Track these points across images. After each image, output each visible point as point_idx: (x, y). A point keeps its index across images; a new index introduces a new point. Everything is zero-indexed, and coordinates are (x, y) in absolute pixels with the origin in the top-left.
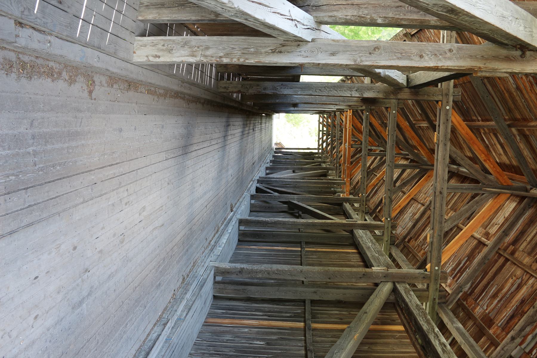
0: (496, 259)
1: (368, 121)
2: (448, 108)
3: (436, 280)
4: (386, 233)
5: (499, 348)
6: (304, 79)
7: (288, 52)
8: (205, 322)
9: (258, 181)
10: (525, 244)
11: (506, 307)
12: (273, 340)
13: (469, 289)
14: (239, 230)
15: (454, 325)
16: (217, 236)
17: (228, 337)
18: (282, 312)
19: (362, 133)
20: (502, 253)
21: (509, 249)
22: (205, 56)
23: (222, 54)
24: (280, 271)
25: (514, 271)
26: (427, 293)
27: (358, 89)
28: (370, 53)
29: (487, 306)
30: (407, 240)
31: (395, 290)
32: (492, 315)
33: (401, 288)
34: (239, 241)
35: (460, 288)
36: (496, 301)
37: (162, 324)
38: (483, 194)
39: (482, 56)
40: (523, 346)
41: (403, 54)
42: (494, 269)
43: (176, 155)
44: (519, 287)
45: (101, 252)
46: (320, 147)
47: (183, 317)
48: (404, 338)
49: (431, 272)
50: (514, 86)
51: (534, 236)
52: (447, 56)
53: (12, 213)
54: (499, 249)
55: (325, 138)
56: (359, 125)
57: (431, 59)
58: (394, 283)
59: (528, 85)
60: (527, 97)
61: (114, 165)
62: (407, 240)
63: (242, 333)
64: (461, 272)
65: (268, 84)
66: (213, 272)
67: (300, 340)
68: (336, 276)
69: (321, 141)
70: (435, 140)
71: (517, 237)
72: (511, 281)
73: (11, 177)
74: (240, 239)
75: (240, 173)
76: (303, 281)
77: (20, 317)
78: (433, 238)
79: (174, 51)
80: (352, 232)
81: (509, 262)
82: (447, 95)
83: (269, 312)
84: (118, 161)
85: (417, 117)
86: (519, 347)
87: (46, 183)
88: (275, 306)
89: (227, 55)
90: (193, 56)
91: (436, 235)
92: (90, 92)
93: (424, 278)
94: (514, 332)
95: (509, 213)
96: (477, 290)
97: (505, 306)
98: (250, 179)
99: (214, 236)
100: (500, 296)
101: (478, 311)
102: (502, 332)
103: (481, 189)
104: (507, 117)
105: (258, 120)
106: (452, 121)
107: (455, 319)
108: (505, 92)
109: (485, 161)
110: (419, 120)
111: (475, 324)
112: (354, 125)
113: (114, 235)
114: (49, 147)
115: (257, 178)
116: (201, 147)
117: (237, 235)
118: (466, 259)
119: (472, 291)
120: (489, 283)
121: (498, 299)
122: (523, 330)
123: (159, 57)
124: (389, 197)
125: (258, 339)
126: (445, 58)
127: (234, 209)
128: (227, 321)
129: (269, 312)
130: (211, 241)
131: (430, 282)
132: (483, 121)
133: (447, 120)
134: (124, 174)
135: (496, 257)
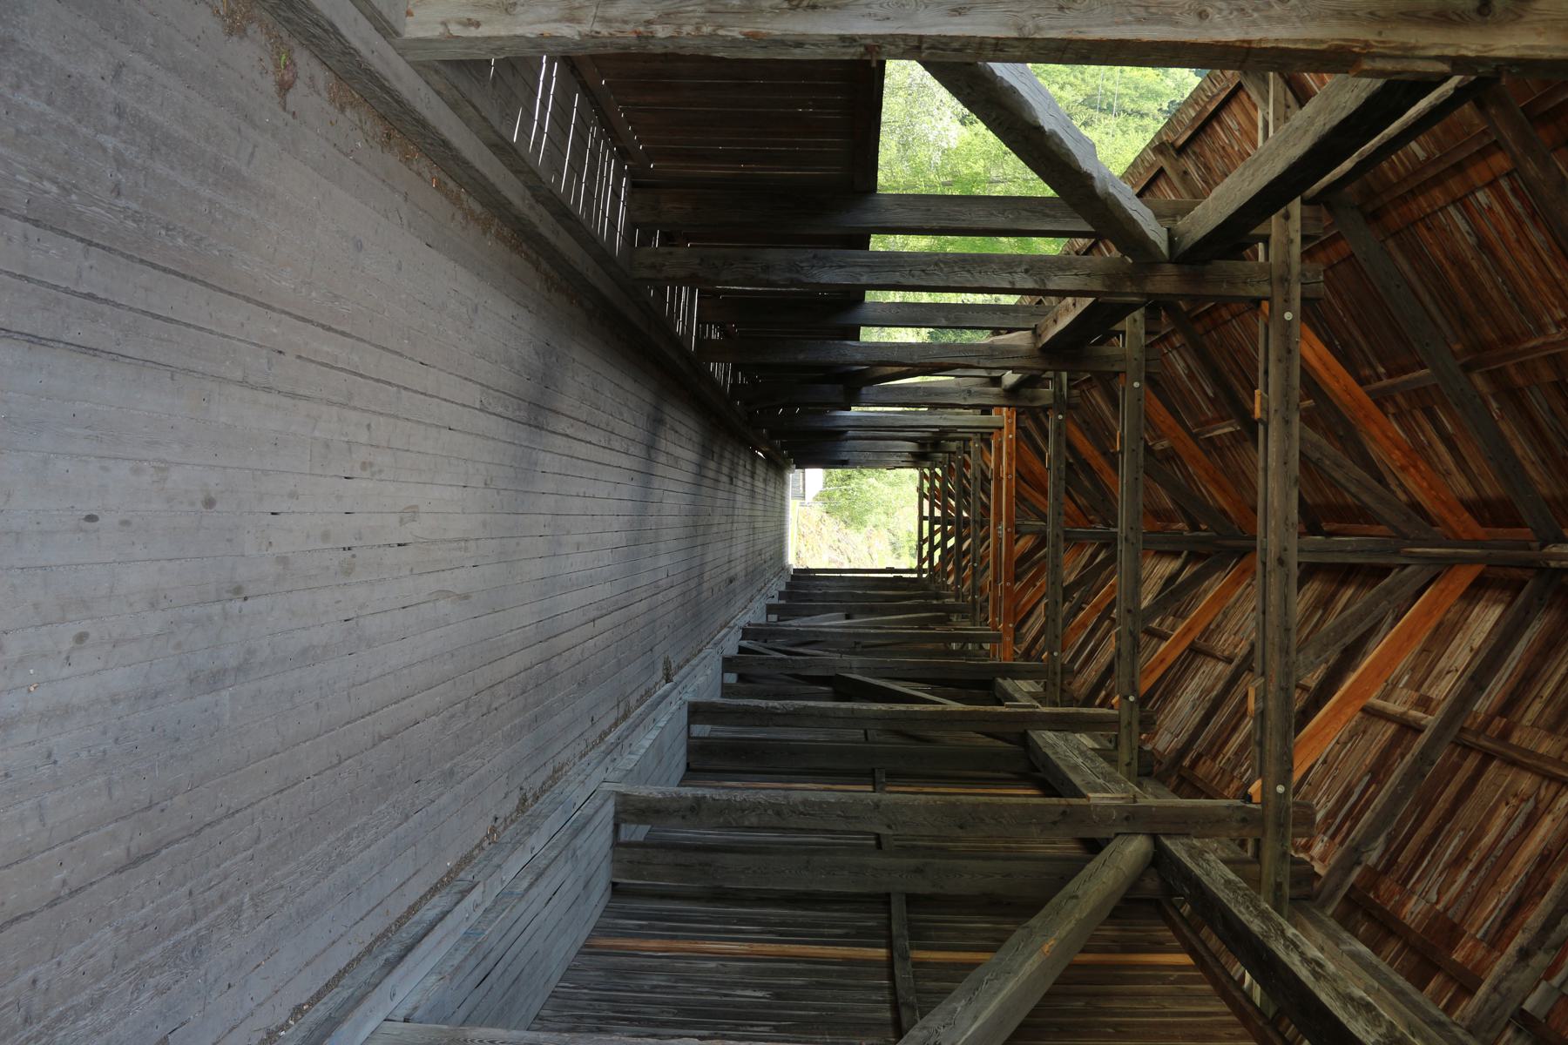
0: (1451, 757)
1: (1063, 439)
2: (1288, 316)
3: (1281, 825)
4: (1124, 741)
5: (1483, 990)
6: (878, 243)
7: (835, 7)
8: (585, 946)
9: (747, 633)
10: (1537, 707)
11: (1495, 883)
12: (794, 987)
13: (1381, 857)
14: (689, 737)
15: (1344, 947)
16: (623, 725)
17: (656, 980)
18: (819, 926)
19: (1044, 493)
20: (1470, 738)
21: (1492, 727)
22: (606, 21)
23: (651, 15)
24: (813, 804)
25: (1512, 782)
26: (1256, 867)
27: (1032, 267)
28: (1061, 8)
29: (1439, 893)
30: (1186, 762)
31: (1159, 859)
32: (1454, 915)
33: (1176, 847)
34: (688, 768)
35: (1353, 856)
36: (1464, 874)
37: (456, 889)
38: (1406, 566)
39: (1371, 13)
40: (1556, 981)
41: (1153, 10)
42: (1452, 789)
43: (509, 414)
44: (1531, 822)
45: (283, 560)
46: (926, 566)
47: (519, 890)
48: (1193, 980)
49: (1264, 802)
50: (1471, 240)
51: (1562, 682)
52: (1272, 13)
53: (40, 283)
54: (1463, 729)
55: (937, 538)
56: (1036, 466)
57: (1229, 22)
58: (1154, 837)
59: (1508, 226)
60: (1509, 264)
61: (336, 331)
62: (1186, 762)
63: (699, 971)
64: (1354, 816)
65: (776, 256)
66: (610, 808)
67: (879, 988)
68: (982, 820)
69: (926, 547)
70: (1258, 414)
71: (1512, 694)
72: (1504, 811)
73: (47, 185)
74: (693, 766)
75: (693, 584)
76: (878, 837)
77: (36, 606)
78: (1264, 698)
79: (519, 9)
80: (1024, 740)
81: (1495, 763)
82: (1284, 280)
83: (776, 924)
84: (348, 330)
85: (1205, 414)
86: (1543, 985)
87: (142, 261)
88: (799, 912)
89: (666, 17)
90: (572, 20)
91: (1272, 688)
92: (284, 87)
93: (1244, 820)
94: (1527, 935)
95: (1484, 636)
96: (1404, 857)
97: (1492, 881)
98: (721, 621)
99: (616, 725)
100: (1475, 857)
101: (1413, 910)
102: (1489, 952)
103: (1397, 552)
104: (1457, 347)
105: (743, 461)
106: (1302, 357)
107: (1345, 935)
108: (1447, 267)
109: (1403, 469)
110: (1208, 422)
111: (1404, 947)
112: (1023, 471)
113: (326, 536)
114: (160, 168)
115: (742, 624)
116: (580, 435)
117: (683, 750)
118: (1366, 779)
119: (1391, 863)
120: (1438, 830)
121: (1470, 867)
122: (1554, 927)
123: (478, 25)
124: (1131, 633)
125: (746, 986)
126: (1268, 18)
127: (675, 679)
128: (653, 944)
129: (781, 924)
130: (606, 734)
131: (1264, 833)
132: (1390, 376)
133: (1289, 351)
134: (361, 376)
135: (1455, 757)
